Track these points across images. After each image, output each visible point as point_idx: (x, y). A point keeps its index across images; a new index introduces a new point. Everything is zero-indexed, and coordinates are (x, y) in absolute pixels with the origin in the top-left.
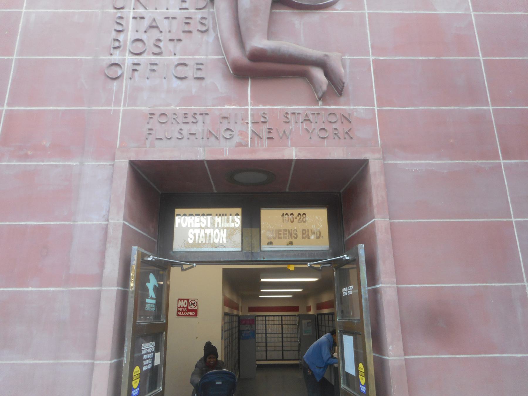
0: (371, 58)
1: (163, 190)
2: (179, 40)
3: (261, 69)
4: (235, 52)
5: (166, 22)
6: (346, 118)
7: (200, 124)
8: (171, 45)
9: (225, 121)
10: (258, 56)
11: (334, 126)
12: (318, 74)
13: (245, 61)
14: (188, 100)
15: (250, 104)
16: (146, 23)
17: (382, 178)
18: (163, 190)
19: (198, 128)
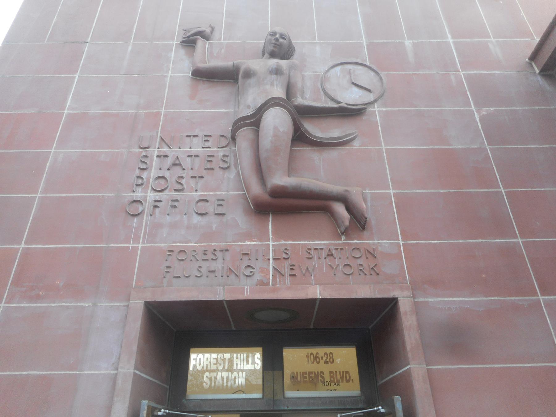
0: (392, 192)
1: (176, 330)
2: (201, 177)
3: (283, 205)
4: (256, 189)
5: (189, 160)
6: (371, 253)
7: (220, 261)
8: (192, 182)
9: (246, 258)
10: (279, 193)
11: (359, 261)
12: (340, 209)
13: (266, 198)
14: (208, 236)
15: (272, 239)
16: (169, 161)
17: (414, 318)
18: (176, 330)
19: (217, 265)
